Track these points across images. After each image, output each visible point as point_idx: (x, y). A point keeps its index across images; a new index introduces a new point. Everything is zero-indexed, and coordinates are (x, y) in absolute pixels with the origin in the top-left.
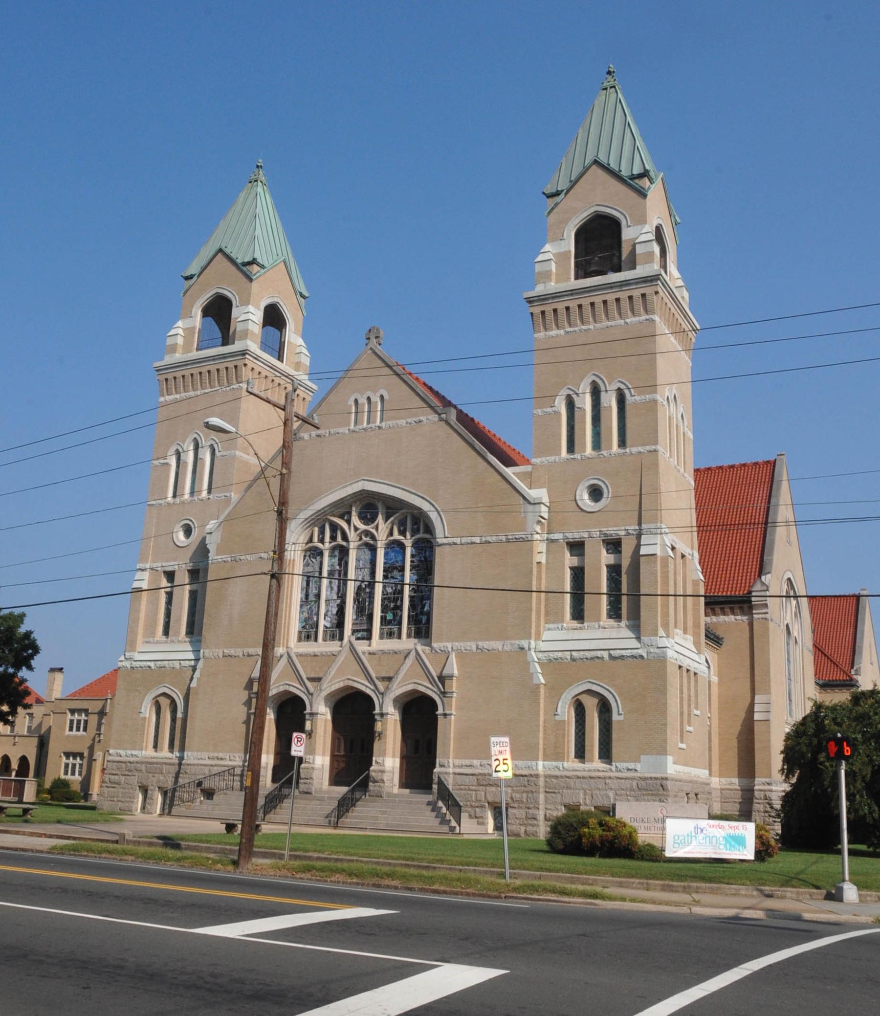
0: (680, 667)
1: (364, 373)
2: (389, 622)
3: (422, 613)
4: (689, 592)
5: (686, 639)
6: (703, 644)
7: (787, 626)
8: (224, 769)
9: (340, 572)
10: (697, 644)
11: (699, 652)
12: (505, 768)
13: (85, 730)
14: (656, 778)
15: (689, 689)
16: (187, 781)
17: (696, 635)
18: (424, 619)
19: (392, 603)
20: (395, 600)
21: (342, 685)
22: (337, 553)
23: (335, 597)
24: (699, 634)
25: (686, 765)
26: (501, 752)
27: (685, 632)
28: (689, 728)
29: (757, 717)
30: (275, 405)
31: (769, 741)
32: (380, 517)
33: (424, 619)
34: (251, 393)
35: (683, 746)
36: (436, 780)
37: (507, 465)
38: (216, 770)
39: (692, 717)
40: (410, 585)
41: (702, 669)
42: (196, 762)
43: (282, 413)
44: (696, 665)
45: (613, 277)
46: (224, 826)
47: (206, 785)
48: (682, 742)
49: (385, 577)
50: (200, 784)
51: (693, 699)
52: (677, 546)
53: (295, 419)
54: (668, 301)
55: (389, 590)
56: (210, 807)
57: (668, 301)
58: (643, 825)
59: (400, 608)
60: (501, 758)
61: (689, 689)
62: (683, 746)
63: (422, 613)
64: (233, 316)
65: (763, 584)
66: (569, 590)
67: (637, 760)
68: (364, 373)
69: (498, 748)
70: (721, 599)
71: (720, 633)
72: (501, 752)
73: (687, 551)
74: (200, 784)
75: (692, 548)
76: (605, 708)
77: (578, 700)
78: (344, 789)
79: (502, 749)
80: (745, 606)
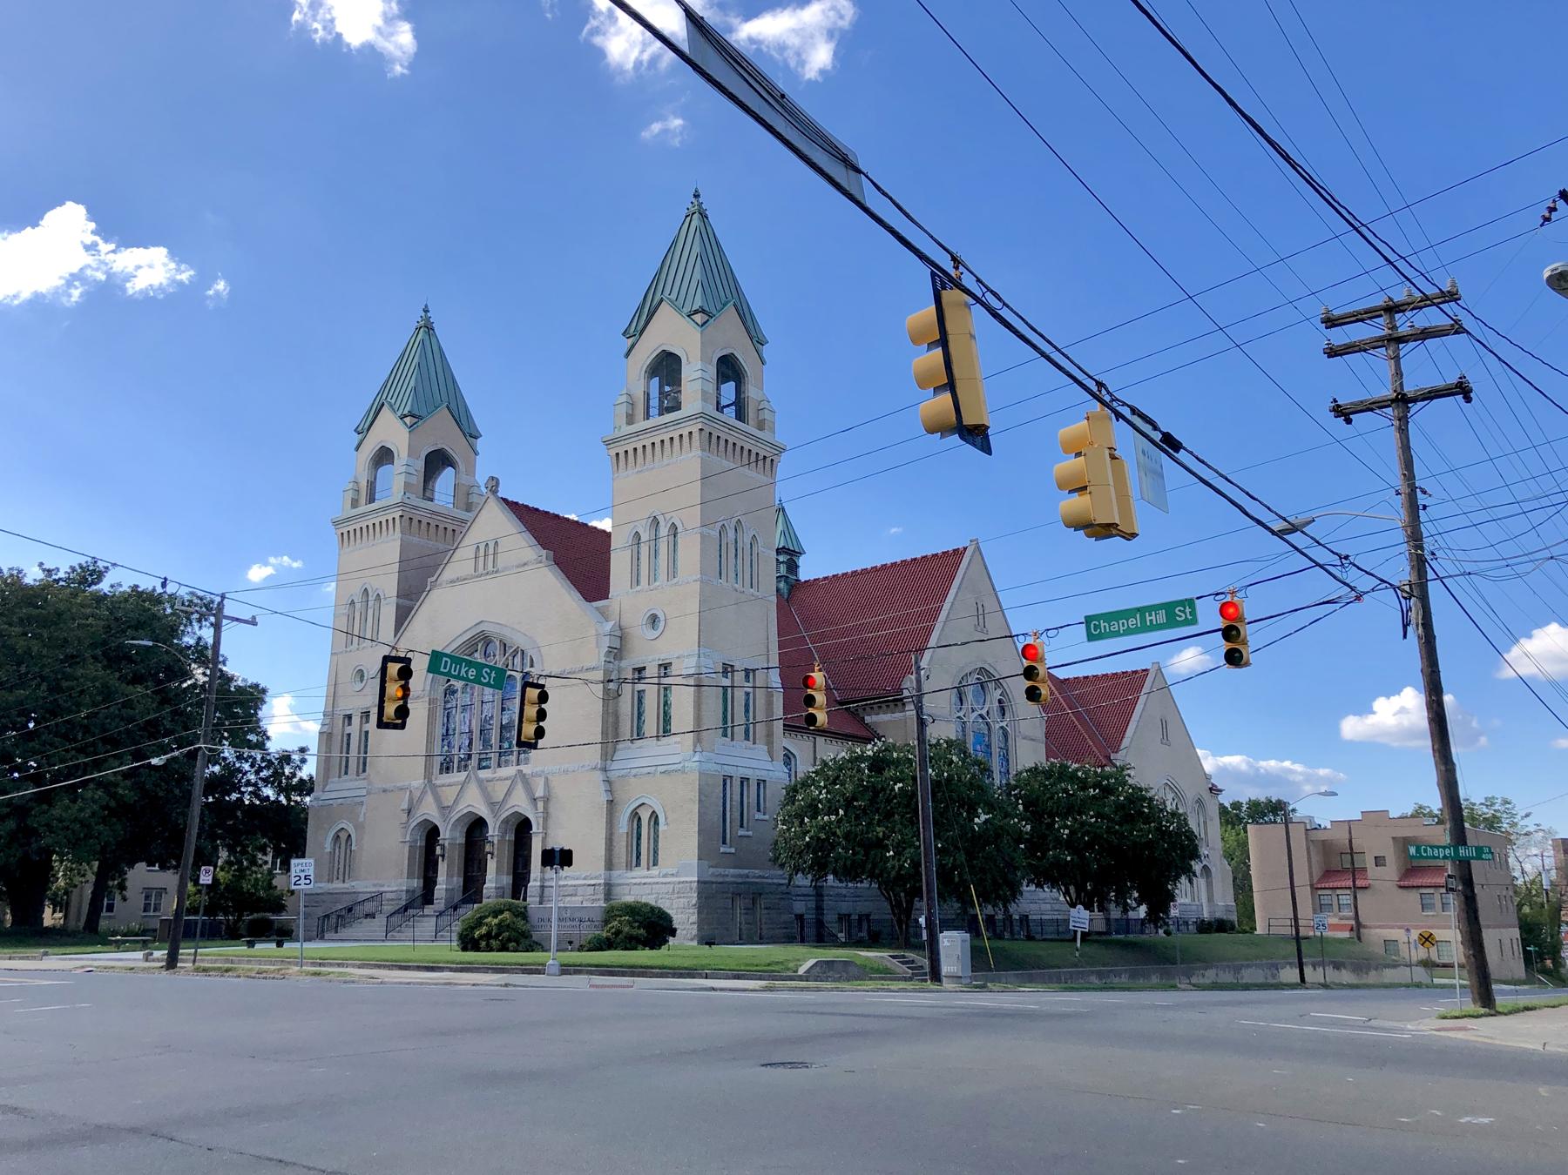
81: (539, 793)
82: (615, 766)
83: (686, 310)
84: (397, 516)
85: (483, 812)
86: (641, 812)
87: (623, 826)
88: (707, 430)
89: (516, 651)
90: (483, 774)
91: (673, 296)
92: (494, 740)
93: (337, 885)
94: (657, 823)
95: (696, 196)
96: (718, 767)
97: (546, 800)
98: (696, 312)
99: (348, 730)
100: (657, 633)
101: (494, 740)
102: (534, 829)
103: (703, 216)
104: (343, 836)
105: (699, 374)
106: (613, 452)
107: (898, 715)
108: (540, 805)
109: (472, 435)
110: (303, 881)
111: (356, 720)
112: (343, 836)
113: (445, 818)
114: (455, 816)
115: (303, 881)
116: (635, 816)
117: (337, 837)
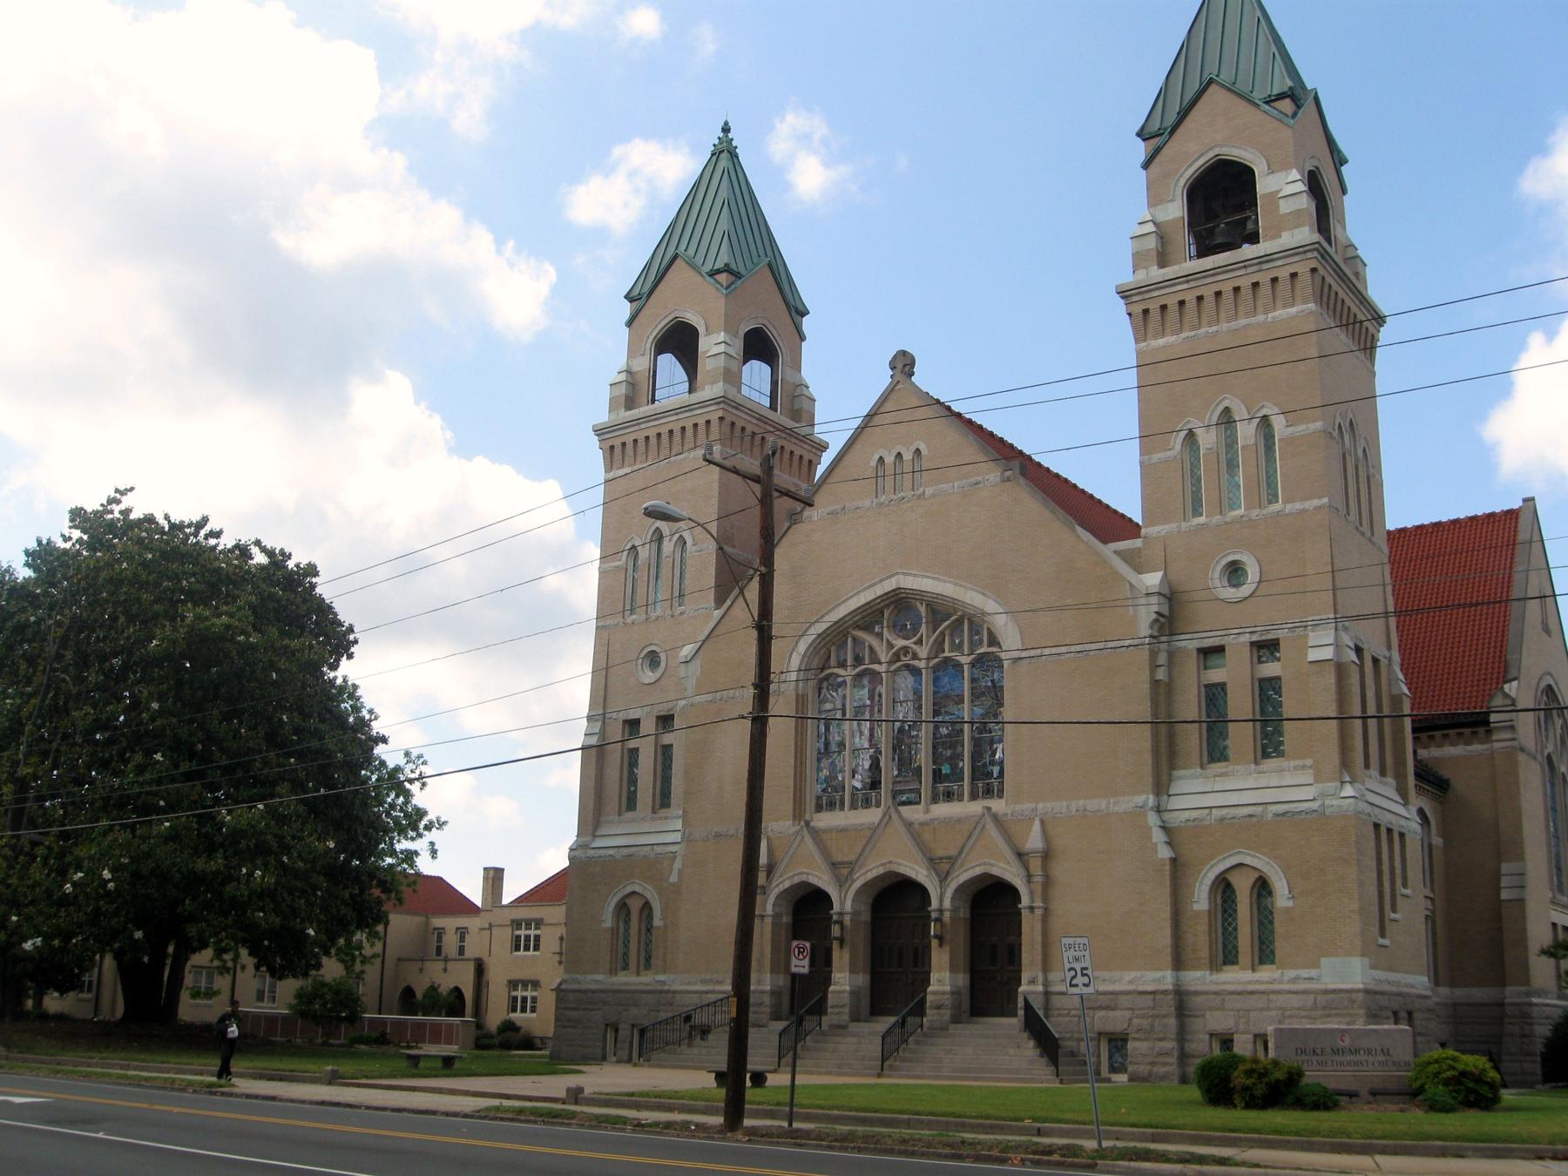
0: (1377, 826)
1: (899, 416)
2: (947, 778)
3: (993, 763)
4: (1386, 711)
5: (1385, 784)
6: (1412, 792)
7: (1549, 757)
8: (721, 996)
9: (872, 706)
10: (1402, 791)
11: (1406, 803)
12: (1086, 980)
13: (536, 948)
14: (1341, 991)
15: (1391, 858)
16: (670, 1015)
17: (1400, 777)
18: (996, 770)
19: (945, 747)
20: (953, 746)
21: (881, 871)
22: (865, 681)
23: (866, 745)
24: (1405, 777)
25: (1391, 970)
26: (1077, 959)
27: (1383, 773)
28: (1393, 916)
29: (1504, 895)
30: (745, 477)
31: (1524, 930)
32: (923, 628)
33: (996, 770)
34: (710, 462)
35: (1386, 942)
36: (1021, 1004)
37: (1105, 541)
38: (713, 997)
39: (1399, 898)
40: (972, 723)
41: (1414, 826)
42: (683, 988)
43: (757, 488)
44: (1403, 822)
45: (1248, 251)
46: (713, 1075)
47: (698, 1019)
48: (1383, 935)
49: (936, 713)
50: (688, 1018)
51: (1398, 871)
52: (1365, 646)
53: (776, 494)
54: (1332, 282)
55: (944, 731)
56: (704, 1051)
57: (1332, 282)
58: (1314, 1058)
59: (960, 757)
60: (1078, 966)
61: (1391, 858)
62: (1386, 942)
63: (993, 763)
64: (701, 349)
65: (1506, 696)
66: (1194, 715)
67: (1315, 964)
68: (899, 416)
69: (1072, 953)
70: (1462, 720)
71: (1445, 773)
72: (1077, 959)
73: (1381, 652)
74: (688, 1018)
75: (1389, 648)
76: (1262, 887)
77: (1225, 879)
78: (888, 1021)
79: (1078, 954)
80: (1481, 730)
81: (1034, 842)
82: (1176, 803)
83: (708, 267)
84: (714, 418)
85: (822, 879)
86: (630, 902)
87: (1201, 899)
88: (729, 419)
89: (960, 621)
90: (913, 813)
91: (691, 252)
92: (923, 758)
93: (625, 979)
94: (650, 917)
95: (726, 129)
96: (1368, 809)
97: (1047, 855)
98: (719, 272)
99: (667, 739)
100: (658, 674)
101: (923, 758)
102: (1025, 901)
103: (733, 155)
104: (635, 906)
105: (722, 348)
106: (1137, 309)
107: (1476, 748)
108: (1036, 865)
109: (798, 311)
110: (1080, 980)
111: (648, 726)
112: (635, 906)
113: (842, 883)
114: (963, 876)
115: (1080, 980)
116: (1224, 887)
117: (623, 907)
